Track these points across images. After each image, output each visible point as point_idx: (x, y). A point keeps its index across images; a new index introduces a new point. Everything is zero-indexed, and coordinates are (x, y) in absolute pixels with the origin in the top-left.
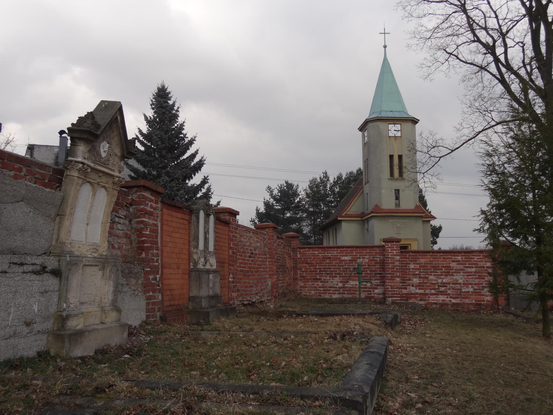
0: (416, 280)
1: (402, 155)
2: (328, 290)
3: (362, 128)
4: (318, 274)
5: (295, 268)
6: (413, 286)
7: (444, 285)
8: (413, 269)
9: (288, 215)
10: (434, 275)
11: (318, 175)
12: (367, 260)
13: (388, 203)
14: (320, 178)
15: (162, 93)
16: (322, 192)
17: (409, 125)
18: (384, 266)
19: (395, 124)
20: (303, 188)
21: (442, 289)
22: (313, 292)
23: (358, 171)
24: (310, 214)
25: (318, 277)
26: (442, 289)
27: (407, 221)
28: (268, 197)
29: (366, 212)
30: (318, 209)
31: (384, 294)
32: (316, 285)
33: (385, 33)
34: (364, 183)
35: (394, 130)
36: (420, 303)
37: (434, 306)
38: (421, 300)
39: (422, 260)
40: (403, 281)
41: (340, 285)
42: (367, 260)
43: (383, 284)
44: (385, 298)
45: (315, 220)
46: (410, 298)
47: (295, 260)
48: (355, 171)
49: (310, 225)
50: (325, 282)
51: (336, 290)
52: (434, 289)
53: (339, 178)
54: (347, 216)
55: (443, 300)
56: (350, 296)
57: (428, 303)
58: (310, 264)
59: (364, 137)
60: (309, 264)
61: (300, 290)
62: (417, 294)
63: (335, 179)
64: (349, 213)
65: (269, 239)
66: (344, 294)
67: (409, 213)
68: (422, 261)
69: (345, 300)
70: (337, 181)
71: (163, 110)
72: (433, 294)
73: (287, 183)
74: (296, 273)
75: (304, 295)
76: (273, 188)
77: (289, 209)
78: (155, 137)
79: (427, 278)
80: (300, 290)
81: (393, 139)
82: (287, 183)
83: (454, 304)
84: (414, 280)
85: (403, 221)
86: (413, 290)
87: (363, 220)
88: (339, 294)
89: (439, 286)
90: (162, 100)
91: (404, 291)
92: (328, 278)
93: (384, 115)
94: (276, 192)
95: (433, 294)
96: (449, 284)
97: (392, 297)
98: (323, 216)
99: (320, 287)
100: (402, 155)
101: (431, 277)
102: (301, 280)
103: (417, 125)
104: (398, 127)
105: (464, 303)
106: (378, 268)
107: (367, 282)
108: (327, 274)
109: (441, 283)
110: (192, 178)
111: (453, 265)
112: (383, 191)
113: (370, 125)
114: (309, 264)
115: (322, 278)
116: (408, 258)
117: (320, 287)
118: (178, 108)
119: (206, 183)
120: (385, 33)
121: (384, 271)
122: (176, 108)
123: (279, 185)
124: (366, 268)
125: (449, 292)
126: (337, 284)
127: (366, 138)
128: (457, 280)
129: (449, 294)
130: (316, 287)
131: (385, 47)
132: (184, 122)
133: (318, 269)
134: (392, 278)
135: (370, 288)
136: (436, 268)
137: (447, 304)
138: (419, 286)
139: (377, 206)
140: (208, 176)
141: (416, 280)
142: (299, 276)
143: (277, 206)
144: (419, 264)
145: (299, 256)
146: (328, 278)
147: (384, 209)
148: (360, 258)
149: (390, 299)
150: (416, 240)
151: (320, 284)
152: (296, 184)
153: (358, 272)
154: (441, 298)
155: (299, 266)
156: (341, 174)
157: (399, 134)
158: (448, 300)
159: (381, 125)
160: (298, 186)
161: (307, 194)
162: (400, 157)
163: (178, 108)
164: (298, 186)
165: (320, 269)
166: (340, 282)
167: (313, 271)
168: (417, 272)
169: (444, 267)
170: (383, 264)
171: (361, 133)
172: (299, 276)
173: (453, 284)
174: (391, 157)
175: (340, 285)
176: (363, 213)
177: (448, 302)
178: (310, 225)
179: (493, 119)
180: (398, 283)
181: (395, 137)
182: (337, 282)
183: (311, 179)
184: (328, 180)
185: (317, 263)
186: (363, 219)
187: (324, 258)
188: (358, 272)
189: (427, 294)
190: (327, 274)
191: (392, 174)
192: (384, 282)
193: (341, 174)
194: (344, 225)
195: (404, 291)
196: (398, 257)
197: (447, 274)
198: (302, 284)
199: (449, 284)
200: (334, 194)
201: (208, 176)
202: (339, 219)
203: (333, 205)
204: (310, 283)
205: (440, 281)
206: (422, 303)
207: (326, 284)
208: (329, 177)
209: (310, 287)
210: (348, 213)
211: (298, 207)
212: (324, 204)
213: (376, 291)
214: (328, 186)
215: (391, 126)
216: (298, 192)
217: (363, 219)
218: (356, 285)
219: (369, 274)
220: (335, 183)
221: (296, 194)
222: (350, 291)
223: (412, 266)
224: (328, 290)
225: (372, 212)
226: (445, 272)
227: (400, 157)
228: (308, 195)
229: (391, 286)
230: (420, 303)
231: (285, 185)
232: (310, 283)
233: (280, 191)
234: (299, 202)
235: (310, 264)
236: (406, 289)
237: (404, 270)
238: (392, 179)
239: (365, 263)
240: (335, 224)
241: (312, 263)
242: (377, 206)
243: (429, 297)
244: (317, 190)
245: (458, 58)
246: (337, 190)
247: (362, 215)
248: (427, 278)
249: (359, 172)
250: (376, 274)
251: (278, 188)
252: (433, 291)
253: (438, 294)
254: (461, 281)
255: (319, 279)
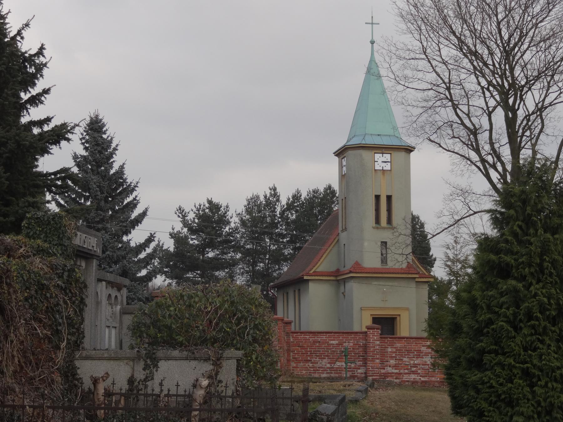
0: (392, 362)
1: (391, 196)
2: (318, 370)
3: (340, 153)
4: (309, 356)
5: (289, 351)
6: (390, 366)
7: (415, 366)
8: (390, 352)
9: (211, 255)
10: (408, 357)
11: (262, 191)
12: (351, 344)
13: (371, 260)
14: (265, 197)
15: (96, 126)
16: (268, 220)
17: (403, 154)
18: (366, 349)
19: (383, 153)
20: (235, 207)
21: (414, 369)
22: (304, 372)
23: (326, 190)
24: (247, 253)
25: (309, 359)
26: (414, 369)
27: (396, 283)
28: (179, 226)
29: (342, 269)
30: (261, 246)
31: (365, 373)
32: (307, 366)
33: (372, 24)
34: (340, 229)
35: (381, 161)
36: (395, 381)
37: (407, 383)
38: (396, 379)
39: (398, 345)
40: (382, 362)
41: (328, 365)
42: (351, 344)
43: (365, 364)
44: (366, 377)
45: (254, 264)
46: (388, 377)
47: (288, 343)
48: (322, 190)
49: (247, 272)
50: (315, 363)
51: (399, 350)
52: (407, 369)
53: (296, 197)
54: (316, 274)
55: (414, 379)
56: (337, 375)
57: (402, 381)
58: (302, 347)
59: (341, 166)
60: (300, 347)
61: (293, 370)
62: (393, 373)
63: (289, 199)
64: (319, 270)
65: (279, 329)
66: (332, 373)
67: (398, 273)
68: (398, 345)
69: (333, 378)
70: (293, 202)
71: (99, 148)
72: (406, 374)
73: (210, 202)
74: (289, 355)
75: (297, 375)
76: (187, 210)
77: (212, 245)
78: (95, 186)
79: (402, 360)
80: (293, 370)
81: (380, 174)
82: (210, 202)
83: (423, 382)
84: (391, 361)
85: (390, 284)
86: (390, 370)
87: (338, 281)
88: (327, 373)
89: (411, 367)
90: (96, 135)
91: (383, 371)
92: (318, 360)
93: (369, 141)
94: (191, 216)
95: (406, 374)
96: (420, 365)
97: (372, 376)
98: (269, 259)
99: (310, 368)
100: (391, 196)
101: (405, 359)
102: (293, 361)
103: (412, 154)
104: (387, 157)
105: (431, 381)
106: (361, 351)
107: (351, 363)
108: (317, 356)
109: (413, 364)
110: (130, 233)
111: (424, 349)
112: (366, 244)
113: (350, 152)
114: (300, 347)
115: (313, 360)
116: (387, 343)
117: (310, 368)
118: (117, 145)
119: (151, 242)
120: (372, 24)
121: (366, 354)
122: (113, 145)
123: (197, 206)
124: (351, 351)
125: (419, 371)
126: (326, 365)
127: (344, 169)
128: (426, 362)
129: (419, 374)
130: (307, 368)
131: (372, 42)
132: (124, 164)
133: (310, 351)
134: (373, 360)
135: (354, 368)
136: (409, 351)
137: (417, 382)
138: (396, 366)
139: (357, 263)
140: (154, 234)
141: (392, 362)
142: (291, 358)
143: (192, 239)
144: (395, 348)
145: (292, 340)
146: (318, 360)
147: (366, 268)
148: (345, 342)
149: (371, 378)
150: (407, 309)
151: (311, 365)
152: (224, 205)
153: (345, 354)
154: (413, 377)
155: (292, 348)
156: (298, 192)
157: (388, 167)
158: (418, 378)
159: (365, 154)
160: (227, 207)
161: (242, 220)
162: (389, 198)
163: (117, 145)
164: (227, 207)
165: (311, 351)
166: (328, 363)
167: (304, 354)
168: (394, 355)
169: (416, 350)
170: (365, 347)
171: (337, 158)
172: (291, 358)
173: (423, 365)
174: (378, 197)
175: (328, 365)
176: (338, 270)
177: (418, 380)
178: (247, 272)
179: (470, 209)
180: (378, 364)
181: (383, 171)
182: (325, 363)
183: (250, 196)
184: (278, 200)
185: (307, 346)
186: (339, 278)
187: (315, 342)
188: (345, 354)
189: (402, 373)
190: (317, 356)
191: (378, 220)
192: (366, 363)
193: (298, 192)
194: (311, 285)
195: (383, 371)
196: (378, 342)
197: (418, 356)
198: (295, 365)
199: (420, 365)
200: (288, 224)
201: (154, 234)
202: (305, 278)
203: (285, 240)
204: (302, 364)
205: (412, 362)
206: (397, 381)
207: (315, 365)
208: (279, 196)
209: (301, 367)
210: (318, 270)
211: (227, 243)
212: (271, 239)
213: (359, 371)
214: (278, 210)
215: (377, 156)
216: (228, 217)
217: (339, 278)
218: (342, 365)
219: (354, 356)
220: (290, 206)
221: (223, 221)
222: (337, 370)
223: (390, 350)
224: (318, 370)
225: (351, 272)
226: (416, 355)
227: (389, 198)
228: (243, 223)
229: (371, 366)
230: (395, 381)
231: (207, 205)
232: (302, 364)
233: (199, 216)
234: (229, 234)
235: (302, 347)
236: (384, 369)
237: (383, 353)
238: (377, 228)
239: (351, 346)
240: (297, 284)
241: (303, 346)
242: (357, 263)
243: (403, 376)
244: (260, 213)
245: (441, 146)
246: (293, 216)
247: (337, 273)
248: (402, 360)
249: (330, 191)
250: (359, 356)
251: (195, 209)
252: (406, 371)
253: (410, 374)
254: (429, 363)
255: (310, 361)
